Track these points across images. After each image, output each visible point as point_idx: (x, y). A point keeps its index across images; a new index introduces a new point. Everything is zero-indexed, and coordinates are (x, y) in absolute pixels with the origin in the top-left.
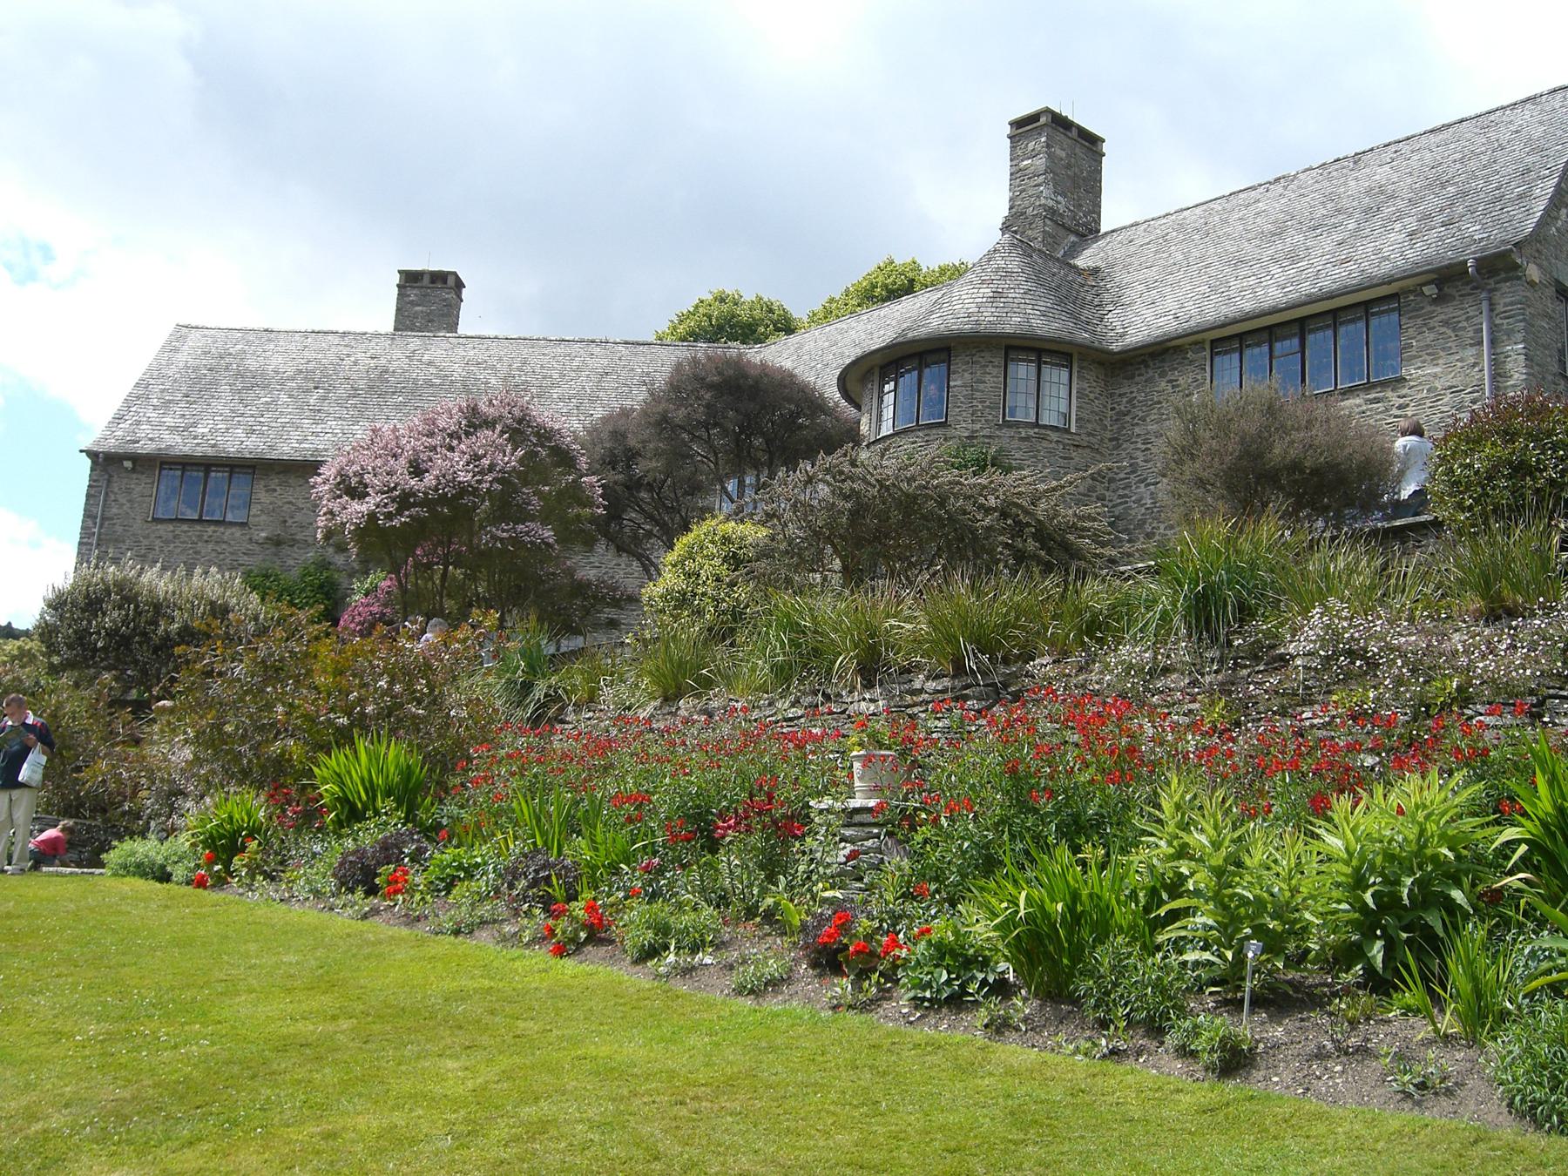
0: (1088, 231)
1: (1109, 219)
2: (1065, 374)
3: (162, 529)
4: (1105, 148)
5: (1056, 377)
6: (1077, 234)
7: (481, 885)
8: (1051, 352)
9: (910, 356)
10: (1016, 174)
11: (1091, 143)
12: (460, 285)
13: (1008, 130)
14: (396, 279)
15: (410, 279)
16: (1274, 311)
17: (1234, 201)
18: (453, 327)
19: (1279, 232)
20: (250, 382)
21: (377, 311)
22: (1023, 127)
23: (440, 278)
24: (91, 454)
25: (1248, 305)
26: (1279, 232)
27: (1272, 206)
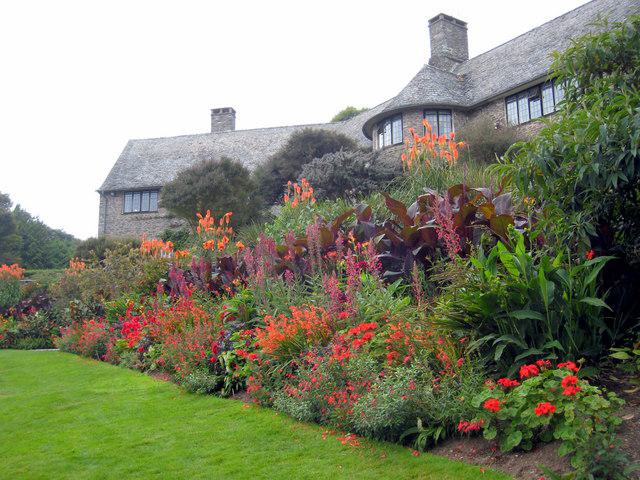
0: (462, 59)
1: (473, 53)
2: (449, 117)
3: (128, 217)
4: (468, 26)
5: (444, 119)
6: (459, 62)
7: (517, 167)
8: (443, 110)
9: (434, 109)
10: (433, 41)
11: (462, 25)
12: (234, 112)
13: (428, 24)
14: (210, 113)
15: (216, 112)
16: (529, 82)
17: (518, 40)
18: (233, 128)
19: (533, 51)
20: (155, 158)
21: (204, 125)
22: (433, 21)
23: (226, 110)
24: (99, 192)
25: (519, 81)
26: (533, 51)
27: (531, 40)
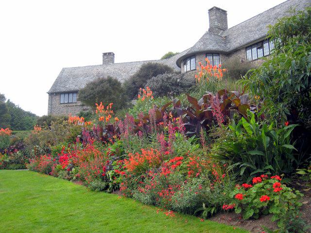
0: (224, 28)
1: (230, 26)
2: (218, 57)
3: (62, 105)
4: (227, 13)
5: (216, 58)
6: (223, 30)
7: (251, 81)
8: (215, 53)
9: (211, 53)
10: (210, 20)
11: (224, 12)
12: (114, 54)
13: (208, 12)
14: (102, 55)
15: (105, 54)
16: (257, 40)
17: (252, 19)
18: (113, 62)
19: (259, 25)
20: (75, 77)
21: (99, 61)
22: (211, 10)
23: (110, 54)
24: (48, 93)
25: (252, 39)
26: (259, 25)
27: (258, 20)
